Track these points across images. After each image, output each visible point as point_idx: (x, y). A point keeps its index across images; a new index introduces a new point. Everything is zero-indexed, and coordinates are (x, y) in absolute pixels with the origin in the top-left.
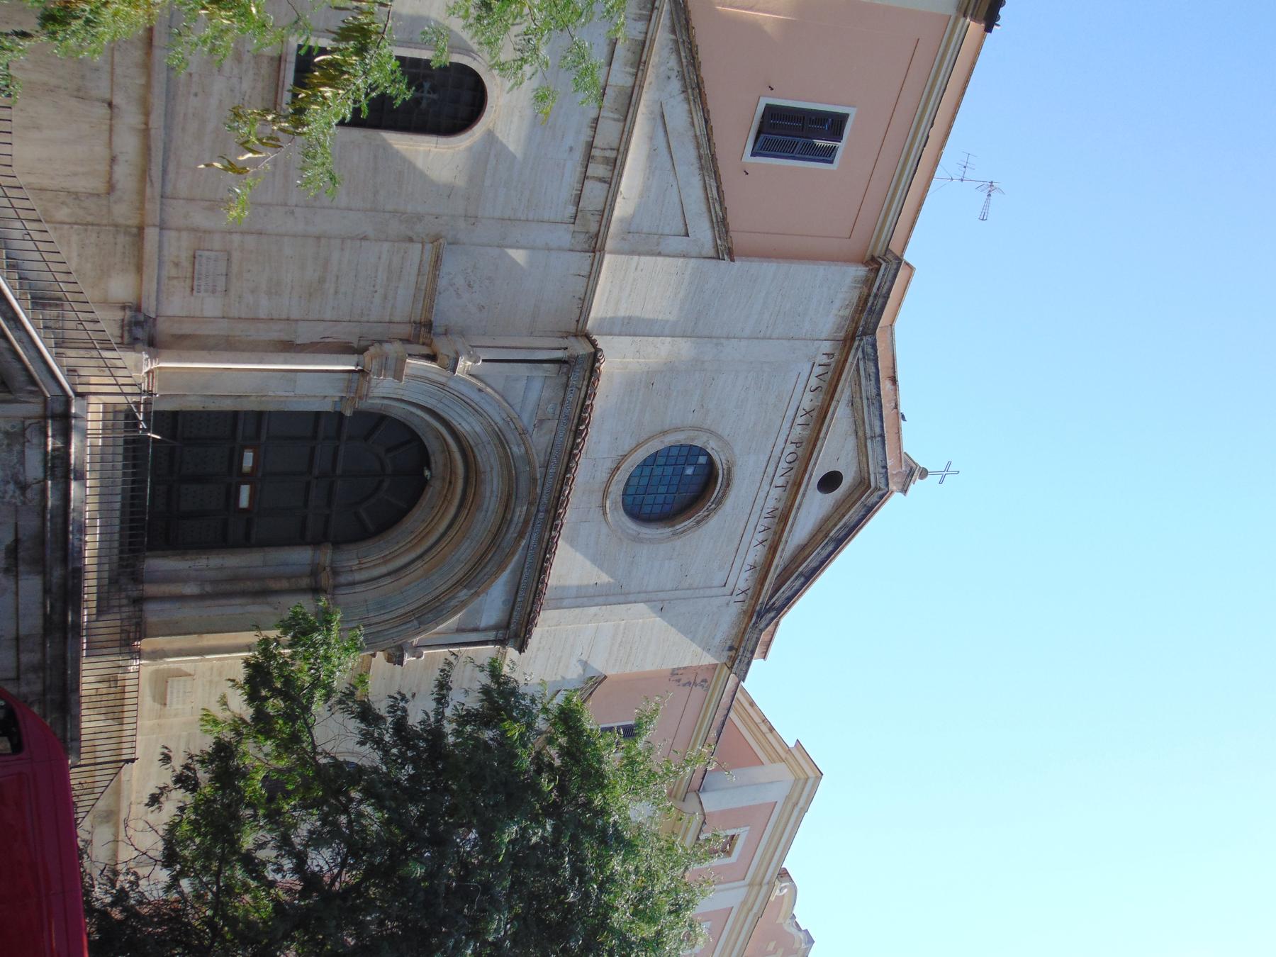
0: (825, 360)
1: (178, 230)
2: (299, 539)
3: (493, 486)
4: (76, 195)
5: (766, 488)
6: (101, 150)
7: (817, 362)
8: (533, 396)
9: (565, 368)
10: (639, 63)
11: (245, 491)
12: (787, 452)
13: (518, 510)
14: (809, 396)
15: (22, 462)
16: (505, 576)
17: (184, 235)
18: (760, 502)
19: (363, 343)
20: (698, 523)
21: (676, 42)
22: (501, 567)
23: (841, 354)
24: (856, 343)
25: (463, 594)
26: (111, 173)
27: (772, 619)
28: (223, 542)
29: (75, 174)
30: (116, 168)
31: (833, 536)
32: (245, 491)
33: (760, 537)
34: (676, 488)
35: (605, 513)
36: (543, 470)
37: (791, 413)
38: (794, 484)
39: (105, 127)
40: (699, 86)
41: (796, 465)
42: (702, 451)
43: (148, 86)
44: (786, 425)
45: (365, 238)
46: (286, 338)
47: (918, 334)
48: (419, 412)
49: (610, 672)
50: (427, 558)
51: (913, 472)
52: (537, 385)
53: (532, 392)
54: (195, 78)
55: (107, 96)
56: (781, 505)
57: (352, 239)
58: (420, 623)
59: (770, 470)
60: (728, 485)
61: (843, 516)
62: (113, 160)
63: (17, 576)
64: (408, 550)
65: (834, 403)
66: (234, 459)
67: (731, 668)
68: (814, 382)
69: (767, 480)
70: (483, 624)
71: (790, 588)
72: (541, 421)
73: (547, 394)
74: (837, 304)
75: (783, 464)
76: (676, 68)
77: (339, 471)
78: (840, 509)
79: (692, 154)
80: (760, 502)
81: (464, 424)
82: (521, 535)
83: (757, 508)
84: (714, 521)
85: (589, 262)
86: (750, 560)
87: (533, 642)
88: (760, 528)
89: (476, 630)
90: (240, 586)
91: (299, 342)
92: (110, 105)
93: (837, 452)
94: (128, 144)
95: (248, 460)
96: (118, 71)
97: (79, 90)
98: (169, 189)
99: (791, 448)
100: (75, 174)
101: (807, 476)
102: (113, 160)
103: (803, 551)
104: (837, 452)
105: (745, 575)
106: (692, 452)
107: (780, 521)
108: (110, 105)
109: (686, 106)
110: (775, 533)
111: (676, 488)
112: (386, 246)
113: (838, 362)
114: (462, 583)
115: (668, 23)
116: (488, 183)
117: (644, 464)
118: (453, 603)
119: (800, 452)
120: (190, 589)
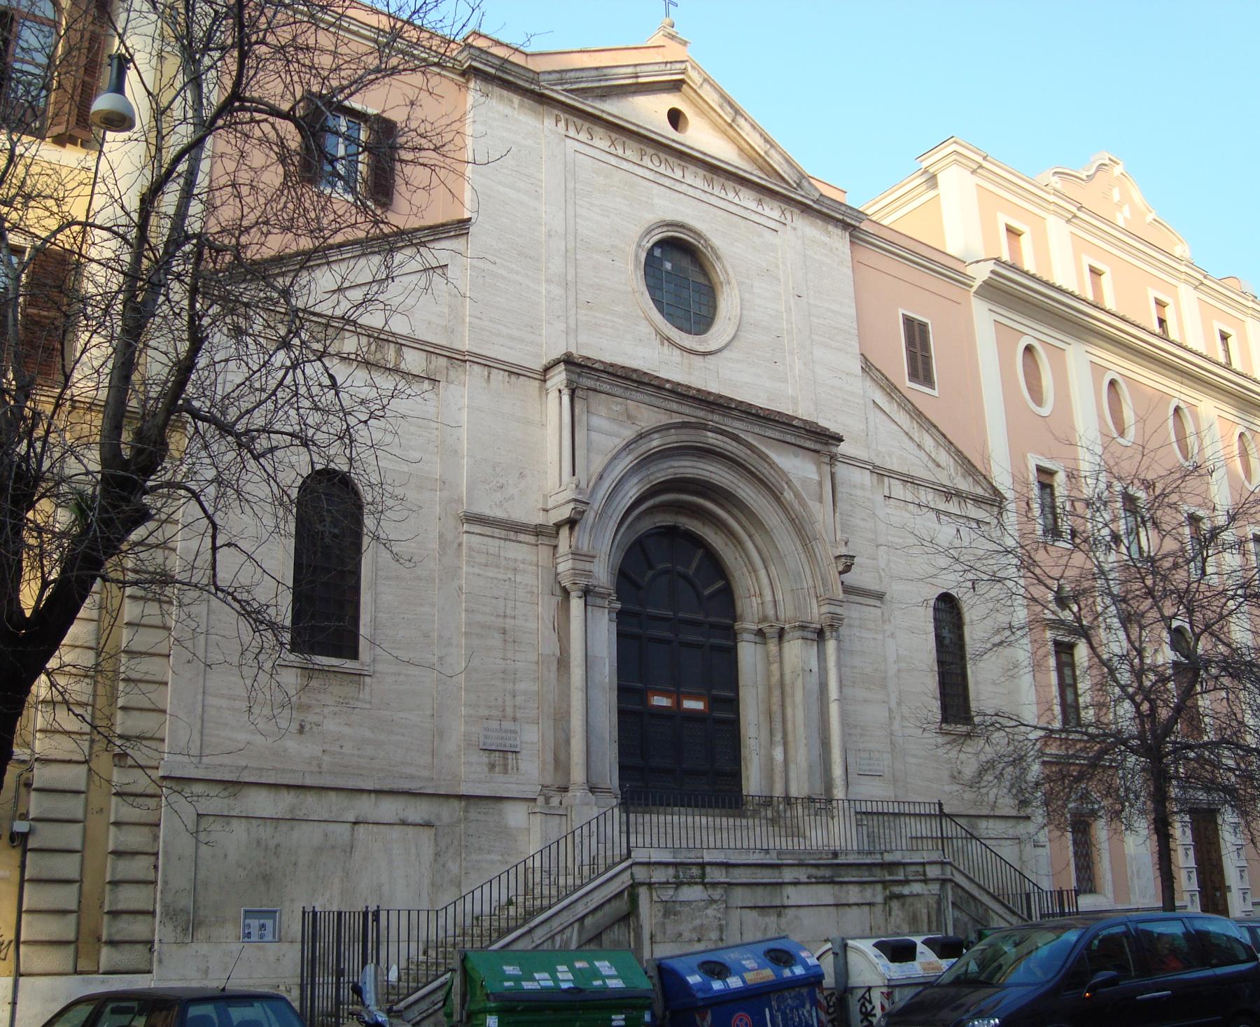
0: (562, 124)
2: (731, 654)
4: (437, 854)
5: (683, 188)
6: (396, 832)
7: (564, 132)
9: (579, 393)
11: (689, 704)
13: (711, 441)
14: (597, 142)
15: (689, 903)
16: (773, 456)
18: (698, 194)
19: (558, 591)
20: (718, 258)
22: (764, 457)
24: (547, 92)
25: (788, 495)
27: (810, 183)
28: (733, 726)
29: (418, 855)
30: (410, 820)
32: (689, 704)
33: (731, 196)
34: (680, 273)
37: (613, 160)
39: (375, 828)
42: (650, 253)
44: (625, 165)
46: (554, 667)
48: (618, 537)
49: (858, 351)
50: (766, 554)
52: (595, 421)
54: (326, 747)
58: (815, 539)
59: (668, 182)
62: (404, 823)
63: (784, 907)
64: (755, 571)
65: (605, 116)
66: (661, 713)
67: (855, 227)
68: (583, 136)
69: (678, 186)
70: (816, 477)
72: (629, 417)
73: (603, 411)
74: (508, 110)
75: (662, 169)
77: (670, 614)
78: (705, 110)
80: (698, 194)
81: (631, 494)
82: (736, 438)
83: (704, 197)
84: (716, 241)
85: (476, 367)
86: (752, 205)
87: (833, 427)
88: (723, 195)
89: (820, 484)
90: (776, 708)
91: (558, 653)
94: (389, 809)
95: (660, 701)
96: (326, 817)
97: (345, 851)
100: (418, 855)
102: (404, 823)
105: (767, 211)
106: (651, 266)
108: (355, 823)
110: (727, 179)
111: (680, 273)
113: (565, 112)
114: (777, 497)
117: (661, 311)
118: (796, 505)
119: (650, 151)
120: (778, 754)
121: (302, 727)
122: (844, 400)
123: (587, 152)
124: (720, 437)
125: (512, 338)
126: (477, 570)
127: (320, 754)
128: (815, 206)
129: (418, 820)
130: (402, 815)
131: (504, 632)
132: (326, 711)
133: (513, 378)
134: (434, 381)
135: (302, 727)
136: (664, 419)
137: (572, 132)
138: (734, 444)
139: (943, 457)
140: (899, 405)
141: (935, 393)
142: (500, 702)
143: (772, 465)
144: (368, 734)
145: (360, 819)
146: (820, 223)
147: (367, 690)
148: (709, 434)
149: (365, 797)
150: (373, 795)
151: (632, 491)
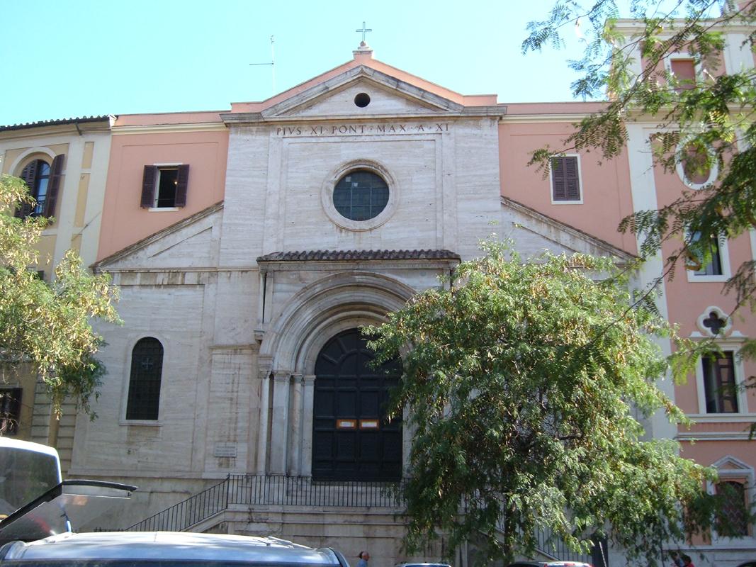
1: (204, 464)
3: (346, 296)
5: (363, 138)
8: (285, 287)
9: (269, 274)
10: (132, 272)
11: (365, 424)
12: (340, 134)
13: (357, 280)
14: (304, 134)
17: (207, 461)
20: (386, 171)
21: (122, 259)
22: (395, 282)
23: (277, 125)
26: (181, 493)
31: (395, 86)
32: (365, 424)
35: (375, 228)
36: (332, 272)
37: (314, 140)
38: (360, 122)
39: (161, 495)
40: (139, 243)
41: (348, 126)
43: (143, 478)
45: (210, 381)
47: (261, 86)
49: (498, 192)
51: (362, 52)
52: (279, 287)
53: (285, 290)
54: (140, 459)
55: (148, 494)
56: (376, 125)
57: (210, 387)
59: (351, 139)
60: (360, 161)
61: (383, 85)
62: (174, 492)
63: (327, 537)
65: (304, 119)
69: (359, 139)
71: (432, 100)
73: (284, 280)
74: (249, 137)
75: (347, 133)
76: (133, 255)
77: (355, 376)
78: (380, 88)
79: (172, 236)
82: (374, 275)
86: (415, 131)
92: (152, 492)
93: (343, 105)
94: (167, 486)
95: (345, 424)
98: (187, 469)
99: (337, 132)
101: (351, 118)
102: (174, 492)
103: (410, 101)
104: (343, 105)
105: (426, 130)
107: (385, 122)
108: (152, 492)
109: (150, 246)
112: (213, 372)
115: (114, 265)
116: (185, 329)
121: (129, 451)
122: (483, 229)
123: (291, 143)
124: (364, 277)
125: (244, 254)
126: (218, 372)
127: (137, 463)
128: (462, 115)
129: (181, 491)
130: (173, 489)
131: (231, 399)
132: (141, 444)
133: (244, 273)
134: (203, 285)
135: (129, 451)
136: (325, 275)
137: (287, 134)
138: (375, 278)
139: (580, 244)
140: (537, 220)
141: (581, 202)
142: (227, 433)
143: (401, 285)
144: (160, 452)
145: (153, 490)
146: (472, 122)
147: (161, 433)
148: (357, 277)
149: (156, 481)
150: (160, 480)
151: (307, 316)
